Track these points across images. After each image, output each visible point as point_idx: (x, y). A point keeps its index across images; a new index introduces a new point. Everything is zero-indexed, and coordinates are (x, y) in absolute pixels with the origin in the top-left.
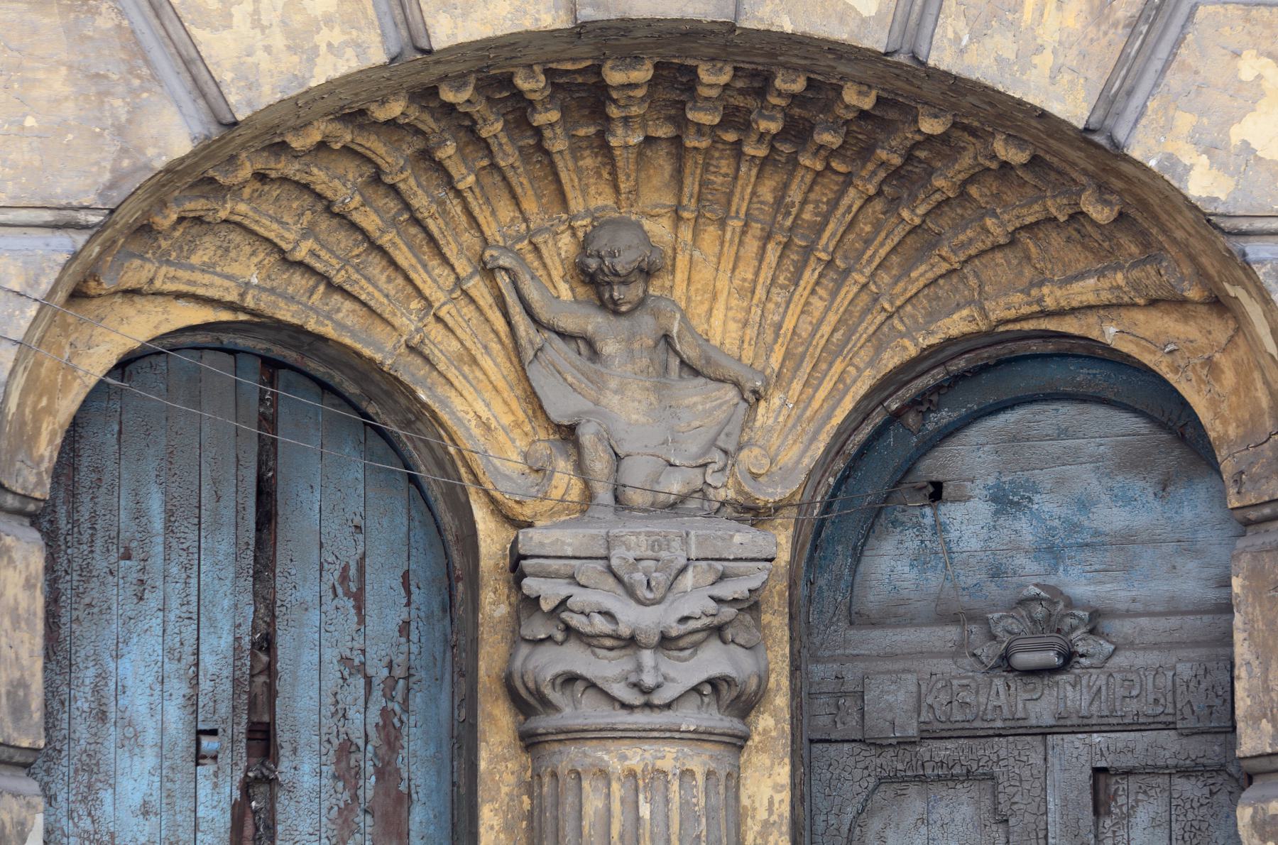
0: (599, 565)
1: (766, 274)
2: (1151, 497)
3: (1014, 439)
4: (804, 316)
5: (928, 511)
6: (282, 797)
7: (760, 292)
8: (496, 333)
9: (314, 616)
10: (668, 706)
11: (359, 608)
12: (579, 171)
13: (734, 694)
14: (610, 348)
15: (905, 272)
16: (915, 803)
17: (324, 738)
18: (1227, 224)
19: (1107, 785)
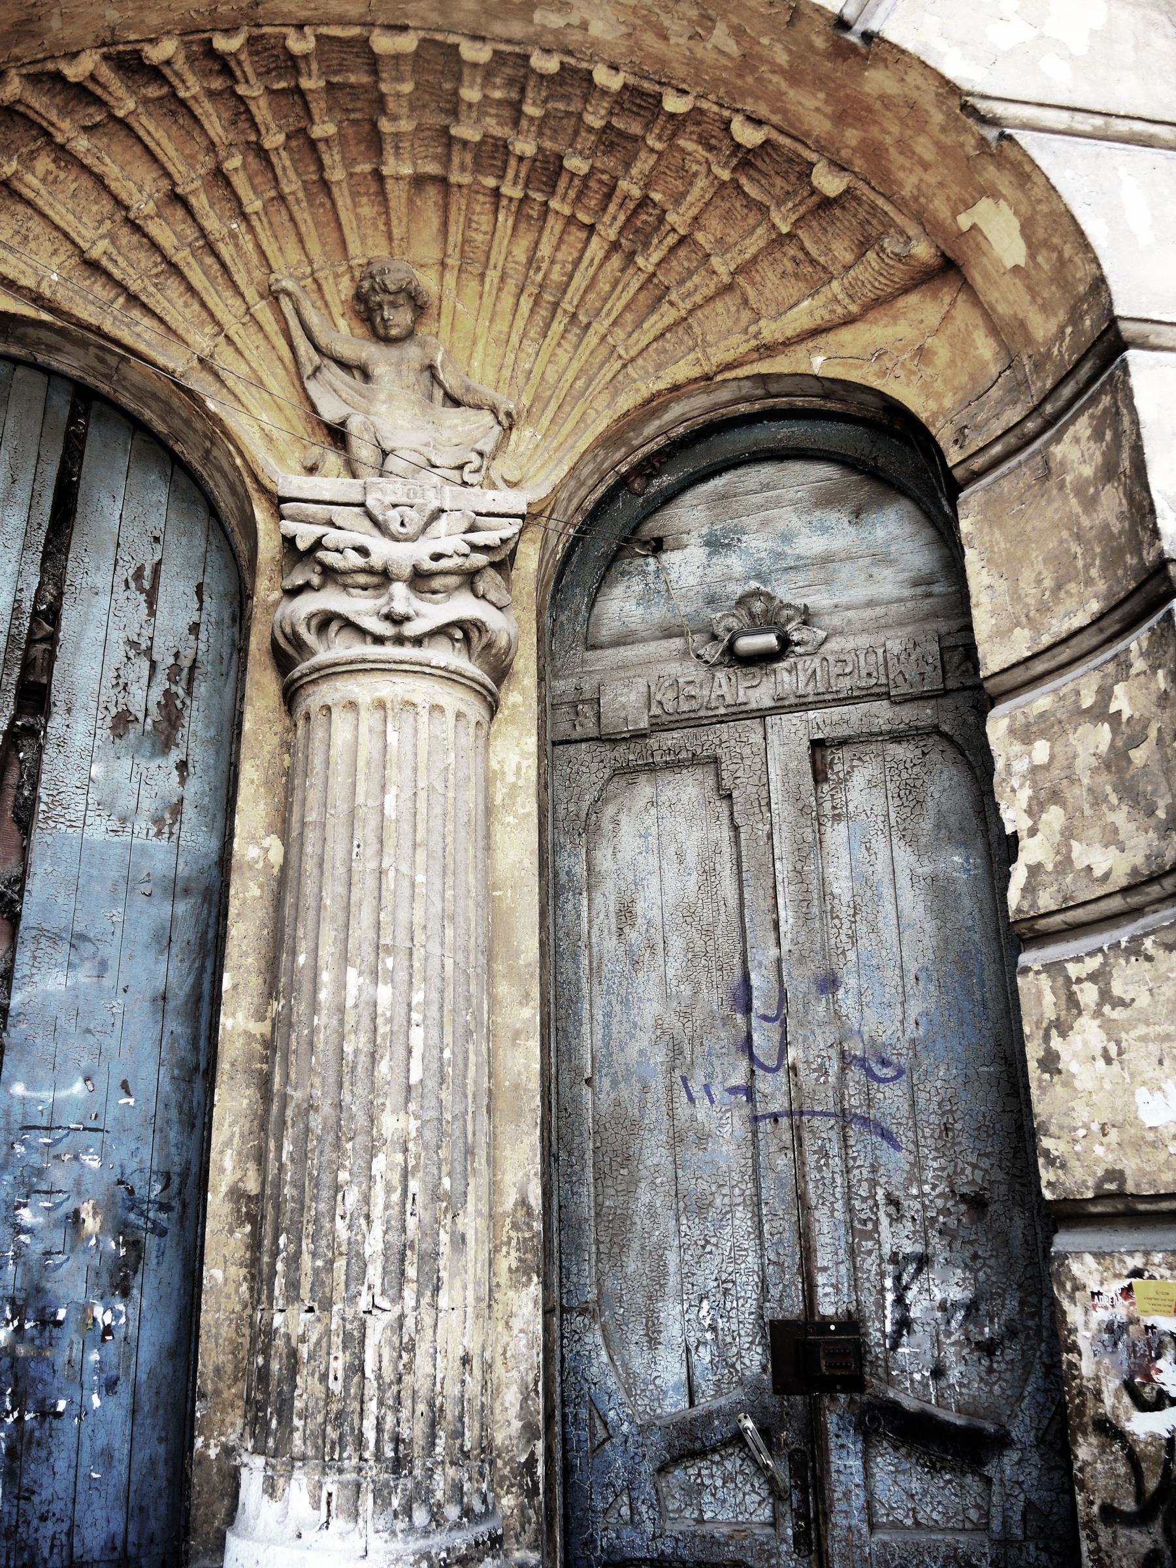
0: (357, 510)
1: (520, 324)
2: (846, 525)
3: (724, 497)
4: (550, 366)
5: (651, 560)
6: (50, 753)
7: (515, 339)
8: (280, 359)
9: (104, 601)
10: (418, 641)
11: (151, 602)
12: (358, 217)
13: (485, 640)
14: (380, 370)
15: (638, 325)
16: (645, 789)
17: (102, 705)
18: (983, 106)
19: (823, 757)
